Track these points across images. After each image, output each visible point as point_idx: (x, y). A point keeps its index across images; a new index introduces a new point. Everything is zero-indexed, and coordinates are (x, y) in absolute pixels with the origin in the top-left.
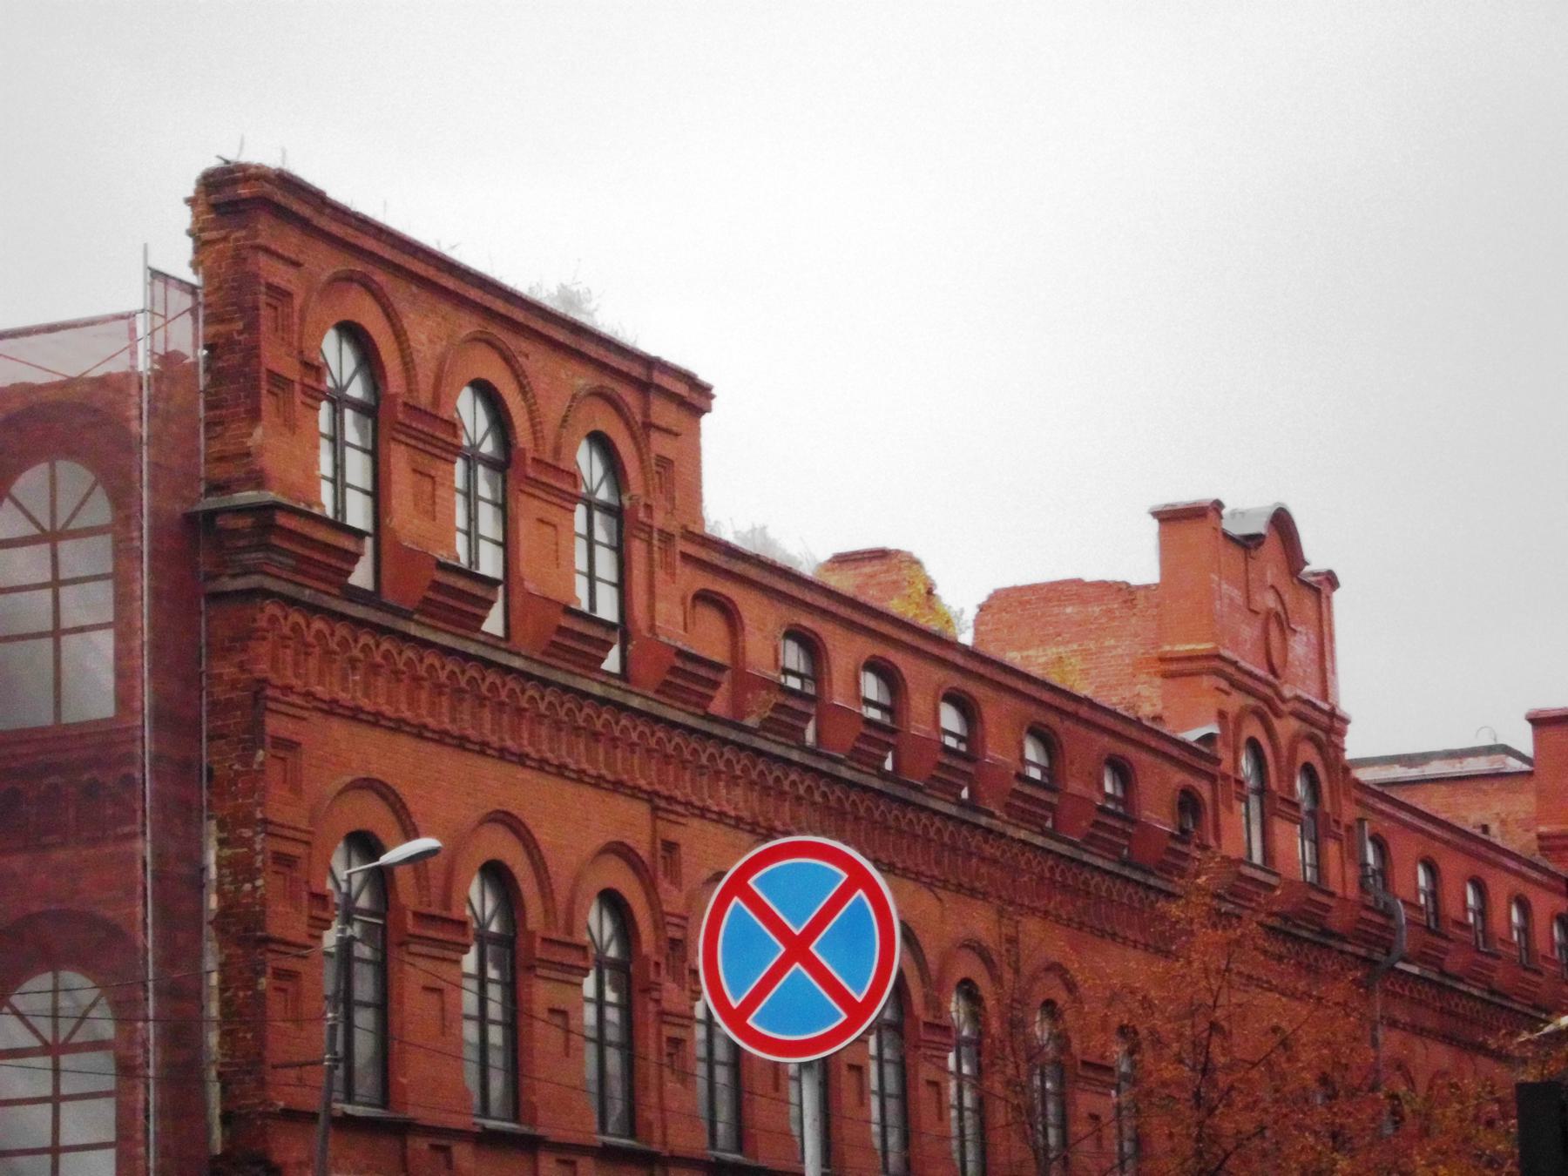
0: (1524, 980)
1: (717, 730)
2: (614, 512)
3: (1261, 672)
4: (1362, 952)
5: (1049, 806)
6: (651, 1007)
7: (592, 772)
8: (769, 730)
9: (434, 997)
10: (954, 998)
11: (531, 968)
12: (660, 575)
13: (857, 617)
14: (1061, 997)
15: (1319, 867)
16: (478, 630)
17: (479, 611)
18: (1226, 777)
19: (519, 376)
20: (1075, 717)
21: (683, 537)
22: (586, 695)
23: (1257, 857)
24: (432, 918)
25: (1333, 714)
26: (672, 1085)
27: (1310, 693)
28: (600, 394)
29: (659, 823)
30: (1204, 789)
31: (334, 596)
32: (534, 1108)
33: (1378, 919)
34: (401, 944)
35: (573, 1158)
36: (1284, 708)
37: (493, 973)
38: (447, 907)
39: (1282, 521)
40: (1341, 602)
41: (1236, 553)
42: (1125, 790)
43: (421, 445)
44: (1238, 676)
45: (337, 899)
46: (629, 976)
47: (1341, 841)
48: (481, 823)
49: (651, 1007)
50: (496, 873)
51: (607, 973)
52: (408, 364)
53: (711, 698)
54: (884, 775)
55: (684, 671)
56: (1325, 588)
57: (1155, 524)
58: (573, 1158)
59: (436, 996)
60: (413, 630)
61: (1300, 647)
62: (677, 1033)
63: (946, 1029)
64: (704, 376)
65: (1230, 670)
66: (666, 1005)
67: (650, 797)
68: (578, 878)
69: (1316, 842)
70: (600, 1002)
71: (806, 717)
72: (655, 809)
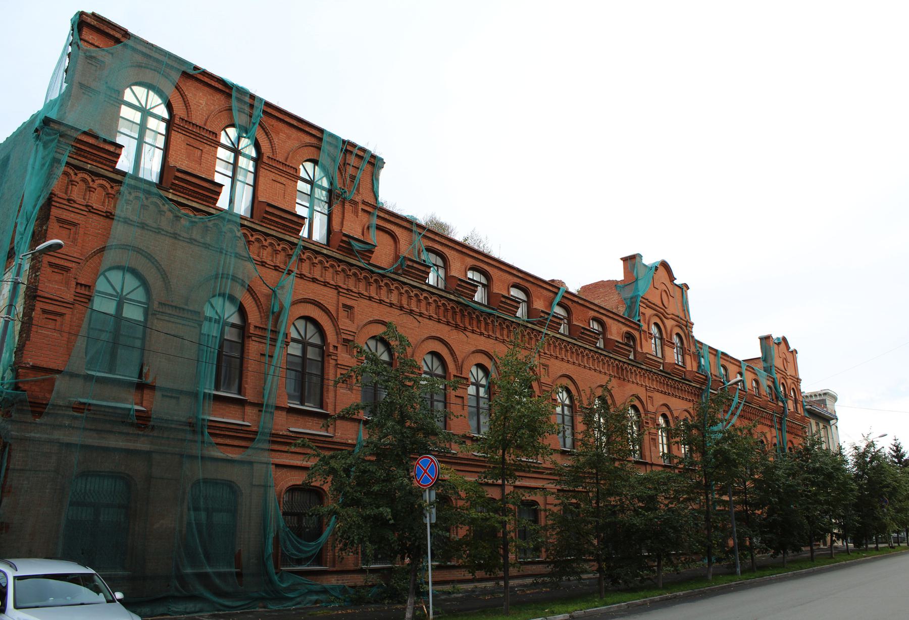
1: (600, 351)
2: (681, 348)
3: (784, 370)
4: (698, 386)
5: (661, 363)
6: (332, 362)
7: (501, 337)
8: (499, 309)
9: (460, 400)
10: (660, 418)
11: (250, 337)
12: (643, 340)
13: (464, 250)
15: (684, 362)
16: (298, 235)
17: (215, 197)
18: (645, 332)
20: (573, 301)
21: (363, 203)
22: (643, 369)
23: (660, 355)
25: (798, 379)
26: (653, 448)
27: (793, 374)
28: (656, 315)
29: (340, 297)
30: (636, 334)
32: (645, 456)
33: (704, 377)
36: (788, 377)
37: (664, 435)
39: (784, 339)
42: (603, 329)
43: (188, 134)
44: (649, 303)
45: (559, 401)
46: (323, 351)
49: (332, 362)
53: (560, 328)
54: (661, 371)
55: (413, 266)
56: (685, 288)
57: (759, 340)
60: (402, 279)
61: (790, 365)
62: (654, 437)
63: (658, 425)
64: (378, 153)
65: (646, 301)
66: (339, 362)
67: (337, 287)
69: (683, 356)
71: (630, 352)
72: (339, 292)
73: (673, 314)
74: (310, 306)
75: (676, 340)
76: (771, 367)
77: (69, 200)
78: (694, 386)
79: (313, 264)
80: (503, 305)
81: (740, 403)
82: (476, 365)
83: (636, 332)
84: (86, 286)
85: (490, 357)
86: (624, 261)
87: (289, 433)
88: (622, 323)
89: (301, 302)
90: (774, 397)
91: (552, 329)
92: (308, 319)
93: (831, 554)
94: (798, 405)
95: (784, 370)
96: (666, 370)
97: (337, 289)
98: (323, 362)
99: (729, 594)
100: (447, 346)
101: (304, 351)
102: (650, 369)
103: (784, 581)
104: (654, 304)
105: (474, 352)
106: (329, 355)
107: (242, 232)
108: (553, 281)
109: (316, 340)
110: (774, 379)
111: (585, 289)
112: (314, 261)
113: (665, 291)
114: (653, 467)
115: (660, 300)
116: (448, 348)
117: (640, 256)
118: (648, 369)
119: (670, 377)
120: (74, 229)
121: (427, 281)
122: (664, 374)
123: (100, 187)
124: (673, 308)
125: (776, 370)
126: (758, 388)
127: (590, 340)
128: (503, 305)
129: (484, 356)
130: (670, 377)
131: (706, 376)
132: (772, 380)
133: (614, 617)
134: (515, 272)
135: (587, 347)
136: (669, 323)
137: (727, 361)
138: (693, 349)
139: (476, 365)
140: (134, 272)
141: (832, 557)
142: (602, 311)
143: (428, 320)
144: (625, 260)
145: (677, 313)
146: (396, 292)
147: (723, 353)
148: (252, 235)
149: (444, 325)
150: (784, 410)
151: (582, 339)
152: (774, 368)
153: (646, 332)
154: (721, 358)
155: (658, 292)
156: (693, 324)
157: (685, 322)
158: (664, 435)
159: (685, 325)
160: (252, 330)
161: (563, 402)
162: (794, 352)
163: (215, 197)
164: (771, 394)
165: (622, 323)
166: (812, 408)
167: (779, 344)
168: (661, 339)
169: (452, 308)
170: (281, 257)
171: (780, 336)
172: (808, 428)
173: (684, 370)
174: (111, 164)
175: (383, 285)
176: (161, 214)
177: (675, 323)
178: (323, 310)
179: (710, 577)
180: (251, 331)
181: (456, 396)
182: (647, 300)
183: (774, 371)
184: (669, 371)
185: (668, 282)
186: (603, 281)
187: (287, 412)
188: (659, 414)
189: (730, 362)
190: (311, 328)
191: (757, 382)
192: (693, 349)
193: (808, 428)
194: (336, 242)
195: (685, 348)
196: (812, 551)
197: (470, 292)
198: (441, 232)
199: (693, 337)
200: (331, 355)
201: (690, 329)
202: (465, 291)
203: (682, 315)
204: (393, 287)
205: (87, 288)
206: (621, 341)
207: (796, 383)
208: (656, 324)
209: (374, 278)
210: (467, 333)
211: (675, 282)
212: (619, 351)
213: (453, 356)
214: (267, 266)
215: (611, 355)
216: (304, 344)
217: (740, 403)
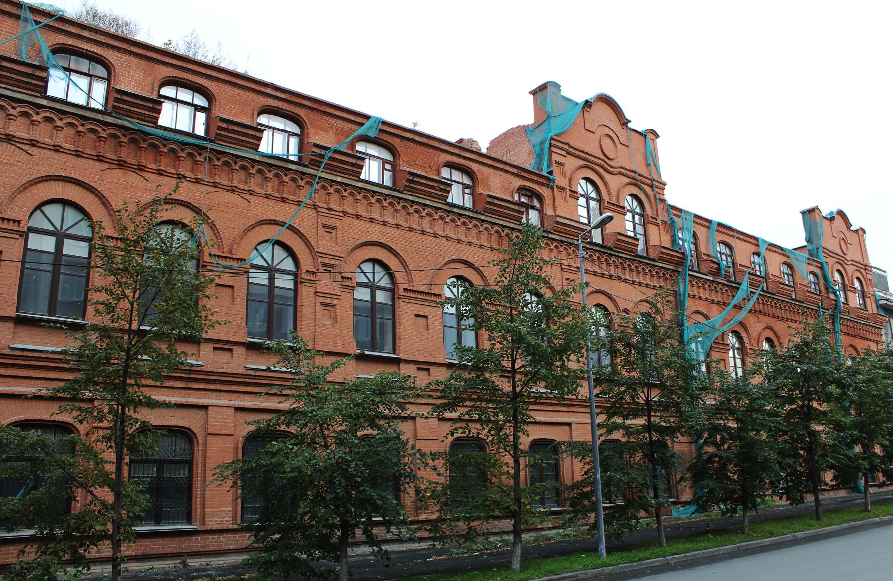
0: (780, 288)
2: (642, 215)
3: (840, 253)
7: (630, 279)
8: (219, 140)
14: (772, 336)
16: (257, 150)
17: (359, 170)
18: (561, 189)
19: (845, 270)
24: (226, 257)
27: (859, 259)
28: (857, 270)
31: (38, 97)
34: (399, 298)
35: (231, 347)
37: (737, 356)
38: (723, 341)
40: (869, 239)
41: (828, 222)
44: (570, 150)
47: (659, 226)
48: (764, 329)
50: (769, 340)
51: (736, 351)
52: (609, 192)
55: (256, 136)
57: (532, 96)
58: (231, 347)
59: (230, 290)
65: (566, 147)
68: (760, 334)
70: (734, 358)
72: (562, 269)
73: (622, 168)
74: (266, 228)
75: (857, 284)
76: (817, 248)
77: (329, 209)
78: (662, 268)
79: (421, 217)
80: (223, 133)
81: (754, 293)
82: (595, 305)
83: (544, 188)
84: (14, 221)
85: (609, 297)
86: (533, 95)
87: (11, 352)
88: (513, 174)
89: (366, 245)
90: (822, 288)
91: (343, 173)
92: (374, 261)
93: (866, 504)
94: (868, 300)
95: (840, 253)
96: (606, 244)
97: (315, 209)
98: (394, 305)
99: (821, 542)
100: (93, 193)
101: (373, 296)
102: (570, 241)
103: (781, 548)
104: (582, 152)
105: (642, 301)
106: (301, 282)
107: (130, 137)
108: (461, 141)
109: (385, 282)
110: (821, 264)
111: (494, 143)
112: (251, 172)
113: (843, 239)
114: (402, 366)
115: (599, 147)
116: (96, 195)
117: (557, 86)
118: (564, 239)
119: (613, 252)
120: (334, 232)
121: (524, 220)
122: (598, 248)
123: (112, 137)
124: (852, 255)
125: (823, 252)
126: (731, 256)
127: (430, 192)
128: (223, 133)
129: (385, 251)
130: (613, 252)
131: (683, 253)
132: (819, 266)
133: (630, 578)
134: (269, 91)
135: (428, 203)
136: (850, 269)
137: (733, 236)
138: (662, 216)
139: (595, 305)
140: (278, 243)
141: (867, 510)
142: (468, 155)
143: (52, 153)
144: (803, 213)
145: (857, 260)
146: (564, 252)
147: (720, 225)
148: (345, 190)
149: (91, 162)
150: (836, 305)
151: (413, 190)
152: (822, 249)
153: (564, 189)
154: (717, 231)
155: (837, 240)
156: (665, 184)
157: (649, 181)
158: (737, 356)
159: (658, 185)
160: (402, 292)
161: (733, 346)
162: (860, 232)
163: (359, 170)
164: (818, 284)
165: (513, 174)
166: (888, 303)
167: (832, 219)
168: (600, 201)
169: (497, 232)
170: (494, 238)
171: (835, 210)
172: (886, 330)
173: (847, 306)
174: (153, 120)
175: (346, 195)
176: (121, 146)
177: (855, 268)
178: (88, 189)
179: (516, 564)
180: (206, 260)
181: (416, 315)
182: (566, 144)
183: (821, 254)
184: (610, 244)
185: (845, 230)
186: (512, 129)
187: (16, 324)
188: (762, 338)
189: (738, 238)
190: (379, 271)
191: (790, 266)
192: (662, 216)
193: (886, 330)
194: (549, 226)
195: (648, 215)
196: (817, 500)
197: (147, 113)
198: (123, 32)
199: (663, 201)
200: (206, 266)
201: (660, 191)
202: (132, 109)
203: (643, 171)
204: (448, 220)
205: (17, 224)
206: (510, 199)
207: (863, 271)
208: (839, 271)
209: (401, 204)
210: (147, 175)
211: (629, 125)
212: (498, 211)
213: (107, 208)
214: (105, 160)
215: (483, 217)
216: (373, 288)
217: (754, 293)
